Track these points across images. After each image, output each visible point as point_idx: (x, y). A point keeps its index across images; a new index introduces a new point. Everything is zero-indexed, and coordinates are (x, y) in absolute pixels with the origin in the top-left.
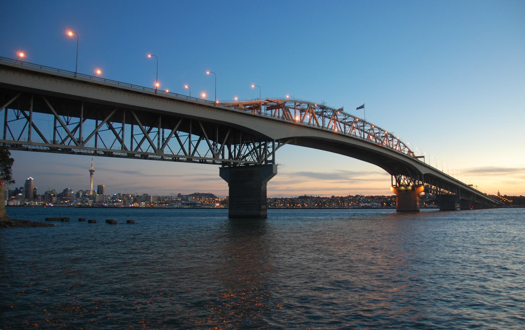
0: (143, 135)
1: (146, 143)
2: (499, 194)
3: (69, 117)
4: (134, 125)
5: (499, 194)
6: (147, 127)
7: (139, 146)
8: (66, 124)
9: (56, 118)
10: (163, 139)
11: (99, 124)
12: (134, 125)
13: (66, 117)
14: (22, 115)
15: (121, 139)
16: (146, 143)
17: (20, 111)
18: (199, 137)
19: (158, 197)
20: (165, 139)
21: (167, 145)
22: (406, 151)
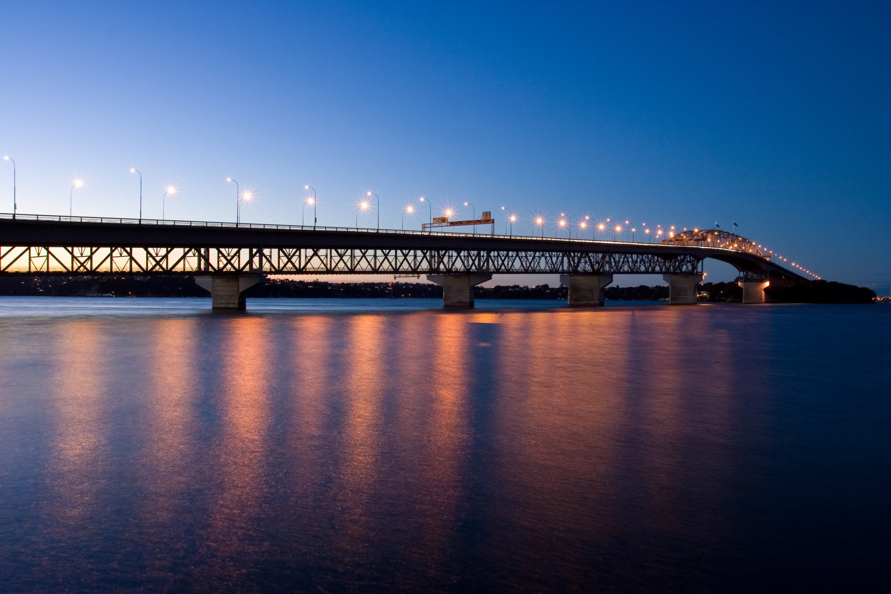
0: (403, 258)
1: (386, 262)
2: (618, 286)
3: (83, 248)
4: (210, 249)
5: (618, 286)
6: (291, 250)
7: (453, 264)
8: (155, 255)
9: (148, 253)
10: (306, 257)
11: (93, 251)
12: (210, 249)
13: (155, 249)
14: (125, 254)
15: (248, 265)
16: (386, 262)
17: (122, 250)
18: (248, 249)
19: (741, 302)
20: (309, 258)
21: (98, 270)
22: (464, 253)
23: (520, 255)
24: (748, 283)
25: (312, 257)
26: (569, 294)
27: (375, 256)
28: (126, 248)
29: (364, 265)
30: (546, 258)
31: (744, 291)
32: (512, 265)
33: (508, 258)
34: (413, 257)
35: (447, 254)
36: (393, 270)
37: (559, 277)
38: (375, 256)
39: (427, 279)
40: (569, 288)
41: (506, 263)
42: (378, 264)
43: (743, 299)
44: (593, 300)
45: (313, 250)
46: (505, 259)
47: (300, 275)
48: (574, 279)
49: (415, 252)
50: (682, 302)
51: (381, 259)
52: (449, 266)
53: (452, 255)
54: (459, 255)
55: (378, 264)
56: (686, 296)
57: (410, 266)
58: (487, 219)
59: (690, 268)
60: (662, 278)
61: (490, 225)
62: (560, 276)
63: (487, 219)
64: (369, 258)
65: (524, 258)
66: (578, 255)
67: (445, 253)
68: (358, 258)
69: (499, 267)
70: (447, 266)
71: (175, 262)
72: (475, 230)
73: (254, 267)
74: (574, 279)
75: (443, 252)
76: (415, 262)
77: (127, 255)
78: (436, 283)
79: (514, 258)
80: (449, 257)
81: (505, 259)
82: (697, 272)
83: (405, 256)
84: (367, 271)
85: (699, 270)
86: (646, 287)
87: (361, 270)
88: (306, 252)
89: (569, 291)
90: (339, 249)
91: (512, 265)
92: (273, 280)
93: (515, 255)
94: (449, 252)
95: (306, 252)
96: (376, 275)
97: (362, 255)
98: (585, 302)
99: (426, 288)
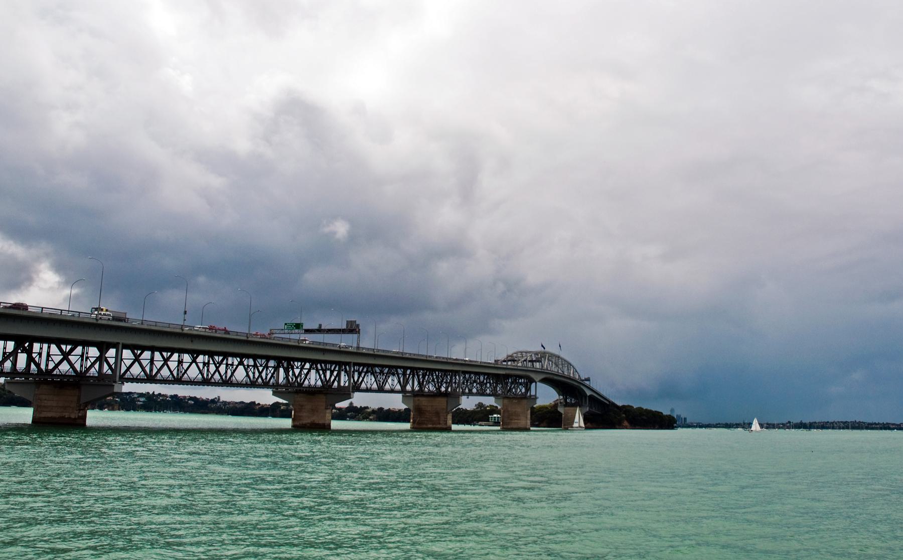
19: (561, 427)
23: (245, 363)
24: (567, 408)
25: (237, 366)
26: (412, 416)
27: (152, 361)
28: (163, 353)
29: (193, 373)
30: (317, 371)
31: (563, 416)
32: (232, 374)
33: (267, 370)
34: (176, 363)
35: (225, 362)
36: (146, 378)
37: (401, 397)
38: (152, 361)
39: (273, 395)
40: (412, 408)
41: (264, 375)
42: (155, 371)
43: (563, 425)
44: (440, 424)
45: (193, 356)
46: (263, 370)
47: (181, 385)
48: (419, 400)
49: (179, 356)
50: (515, 426)
51: (158, 364)
52: (226, 377)
53: (233, 363)
54: (194, 361)
55: (155, 371)
56: (519, 421)
57: (171, 372)
58: (352, 329)
59: (523, 390)
60: (494, 400)
61: (355, 336)
62: (403, 396)
63: (352, 329)
64: (144, 363)
65: (251, 367)
66: (359, 369)
67: (222, 360)
68: (128, 363)
69: (210, 376)
70: (224, 377)
71: (133, 366)
72: (376, 346)
73: (342, 384)
74: (419, 400)
75: (221, 358)
76: (178, 370)
77: (162, 360)
78: (287, 401)
79: (235, 367)
80: (227, 365)
81: (263, 370)
82: (531, 396)
83: (166, 361)
84: (196, 382)
85: (533, 393)
86: (275, 403)
87: (189, 380)
88: (49, 347)
89: (412, 413)
90: (216, 355)
91: (232, 374)
92: (171, 397)
93: (236, 363)
94: (227, 360)
95: (49, 347)
96: (177, 385)
97: (169, 363)
98: (430, 426)
99: (186, 400)
